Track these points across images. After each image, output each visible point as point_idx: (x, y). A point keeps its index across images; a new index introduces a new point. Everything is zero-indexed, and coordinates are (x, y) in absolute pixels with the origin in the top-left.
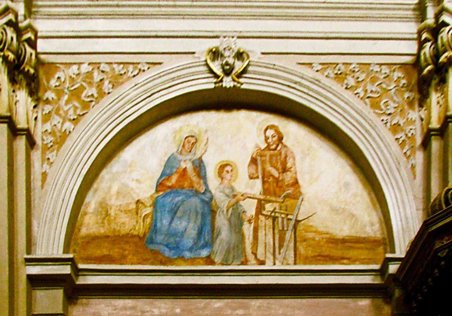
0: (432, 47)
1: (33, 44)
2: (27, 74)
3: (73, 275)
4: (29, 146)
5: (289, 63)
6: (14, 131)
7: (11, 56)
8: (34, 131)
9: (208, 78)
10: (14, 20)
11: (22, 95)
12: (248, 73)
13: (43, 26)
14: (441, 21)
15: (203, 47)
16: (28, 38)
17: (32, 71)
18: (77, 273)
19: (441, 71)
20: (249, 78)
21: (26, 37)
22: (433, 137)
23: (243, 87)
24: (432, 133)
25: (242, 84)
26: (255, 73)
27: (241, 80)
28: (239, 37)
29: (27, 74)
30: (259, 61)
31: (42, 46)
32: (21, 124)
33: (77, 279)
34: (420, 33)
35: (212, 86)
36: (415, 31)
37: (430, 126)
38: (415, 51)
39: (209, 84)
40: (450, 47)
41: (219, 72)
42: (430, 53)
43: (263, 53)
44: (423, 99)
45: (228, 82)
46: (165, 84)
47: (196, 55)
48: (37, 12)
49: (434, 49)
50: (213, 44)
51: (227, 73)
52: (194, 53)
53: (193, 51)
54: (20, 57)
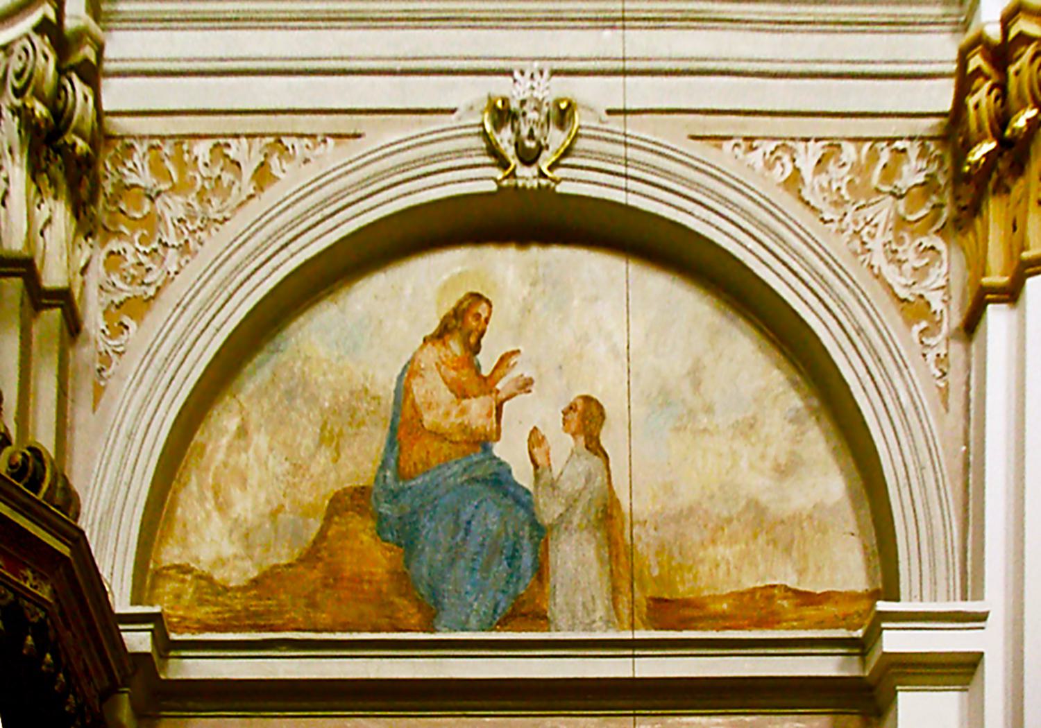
0: (995, 92)
1: (92, 75)
2: (68, 156)
3: (156, 658)
4: (66, 335)
5: (671, 133)
6: (40, 297)
7: (40, 110)
8: (82, 293)
9: (484, 165)
10: (93, 59)
11: (59, 211)
12: (574, 156)
13: (122, 46)
14: (1013, 33)
15: (469, 96)
16: (76, 57)
17: (82, 146)
18: (163, 653)
19: (1014, 153)
20: (573, 167)
21: (77, 58)
22: (990, 307)
23: (560, 189)
24: (989, 297)
25: (557, 182)
26: (587, 153)
27: (559, 173)
28: (555, 73)
29: (68, 156)
30: (601, 126)
31: (115, 94)
32: (53, 277)
33: (164, 667)
34: (963, 59)
35: (492, 187)
36: (954, 54)
37: (985, 281)
38: (947, 105)
39: (485, 181)
40: (1034, 98)
41: (510, 152)
42: (989, 110)
43: (609, 112)
44: (966, 217)
45: (527, 176)
46: (727, 207)
47: (457, 114)
48: (112, 13)
49: (997, 98)
50: (500, 87)
51: (529, 158)
52: (453, 111)
53: (452, 106)
54: (61, 116)
